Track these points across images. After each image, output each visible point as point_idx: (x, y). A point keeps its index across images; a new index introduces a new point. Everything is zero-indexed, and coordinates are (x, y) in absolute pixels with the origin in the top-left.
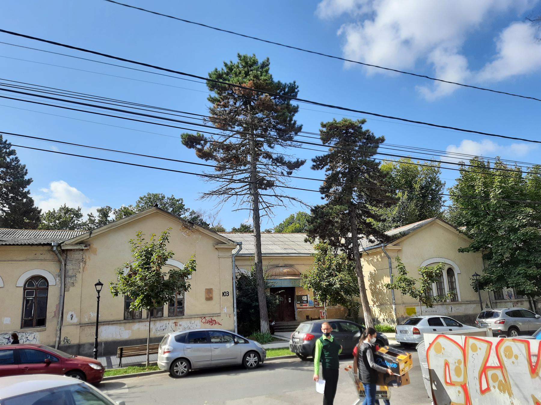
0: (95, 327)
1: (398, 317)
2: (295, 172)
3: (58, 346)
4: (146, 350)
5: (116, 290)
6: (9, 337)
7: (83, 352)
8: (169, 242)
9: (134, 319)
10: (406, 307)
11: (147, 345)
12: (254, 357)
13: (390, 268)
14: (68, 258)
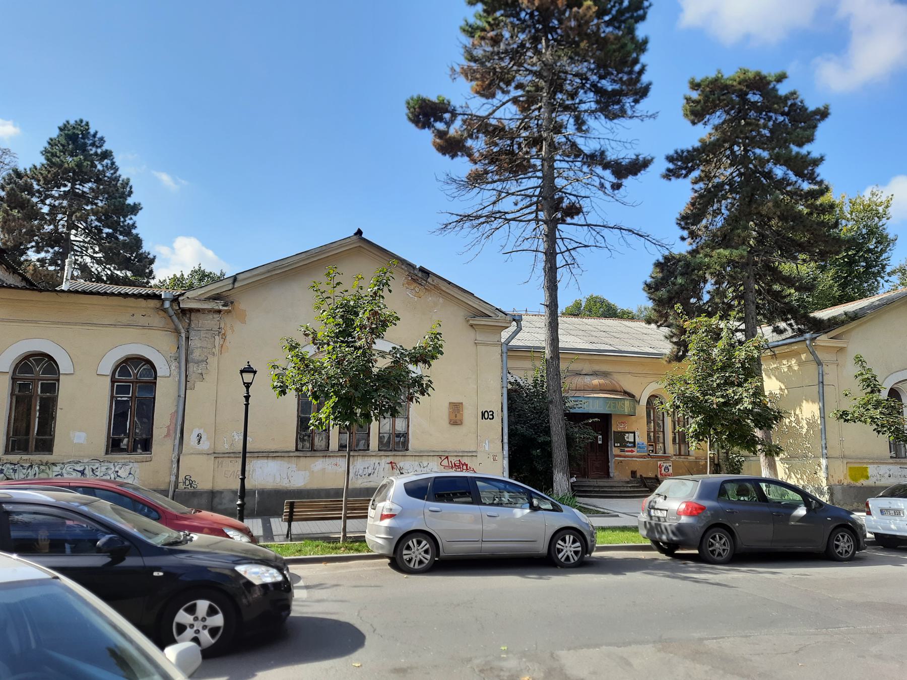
0: (240, 461)
1: (833, 483)
2: (629, 182)
3: (175, 491)
4: (341, 510)
5: (282, 382)
6: (84, 469)
7: (220, 507)
8: (390, 291)
9: (315, 451)
10: (849, 465)
11: (344, 499)
12: (574, 542)
13: (821, 385)
14: (193, 325)
